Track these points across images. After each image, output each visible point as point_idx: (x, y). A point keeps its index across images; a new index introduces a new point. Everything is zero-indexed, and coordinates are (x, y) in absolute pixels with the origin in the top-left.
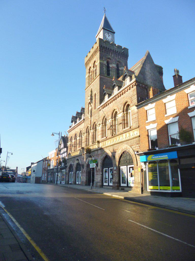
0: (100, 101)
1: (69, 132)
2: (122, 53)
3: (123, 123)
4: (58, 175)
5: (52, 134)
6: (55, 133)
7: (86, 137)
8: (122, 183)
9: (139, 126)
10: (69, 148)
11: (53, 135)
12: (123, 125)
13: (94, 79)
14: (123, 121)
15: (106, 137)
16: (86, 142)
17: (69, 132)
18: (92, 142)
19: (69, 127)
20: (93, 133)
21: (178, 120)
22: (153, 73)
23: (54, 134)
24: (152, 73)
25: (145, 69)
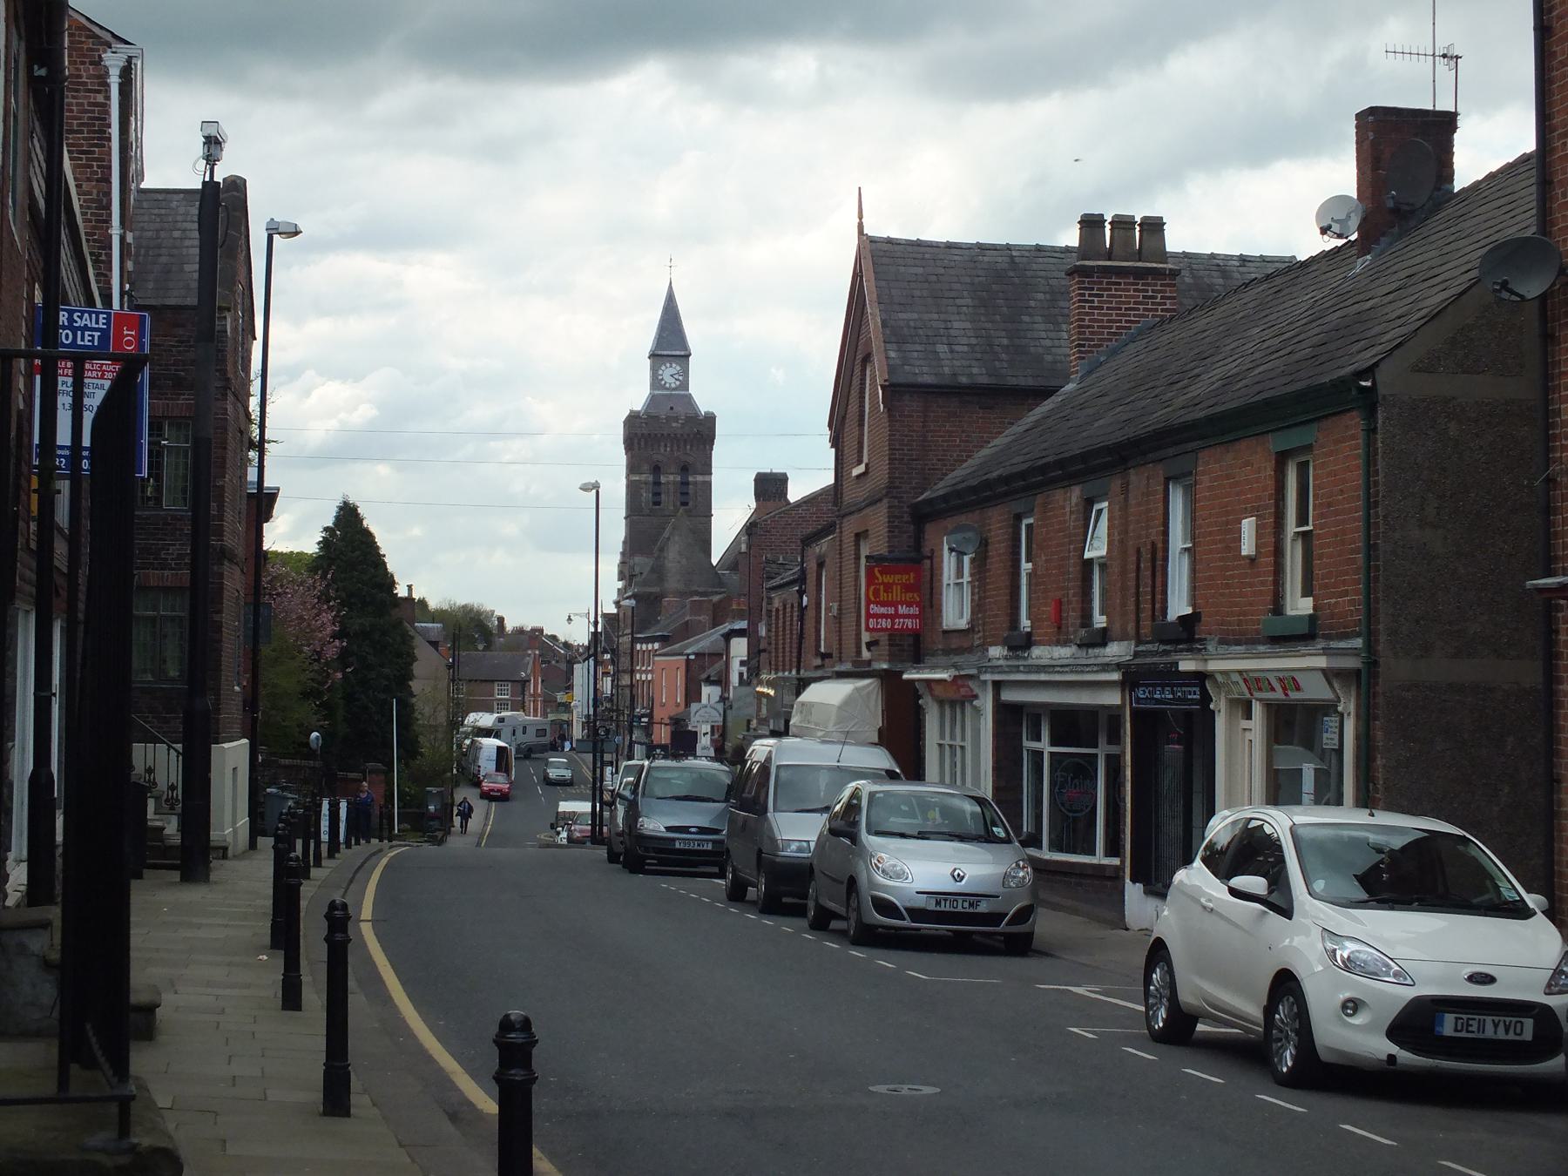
11: (569, 619)
25: (664, 558)
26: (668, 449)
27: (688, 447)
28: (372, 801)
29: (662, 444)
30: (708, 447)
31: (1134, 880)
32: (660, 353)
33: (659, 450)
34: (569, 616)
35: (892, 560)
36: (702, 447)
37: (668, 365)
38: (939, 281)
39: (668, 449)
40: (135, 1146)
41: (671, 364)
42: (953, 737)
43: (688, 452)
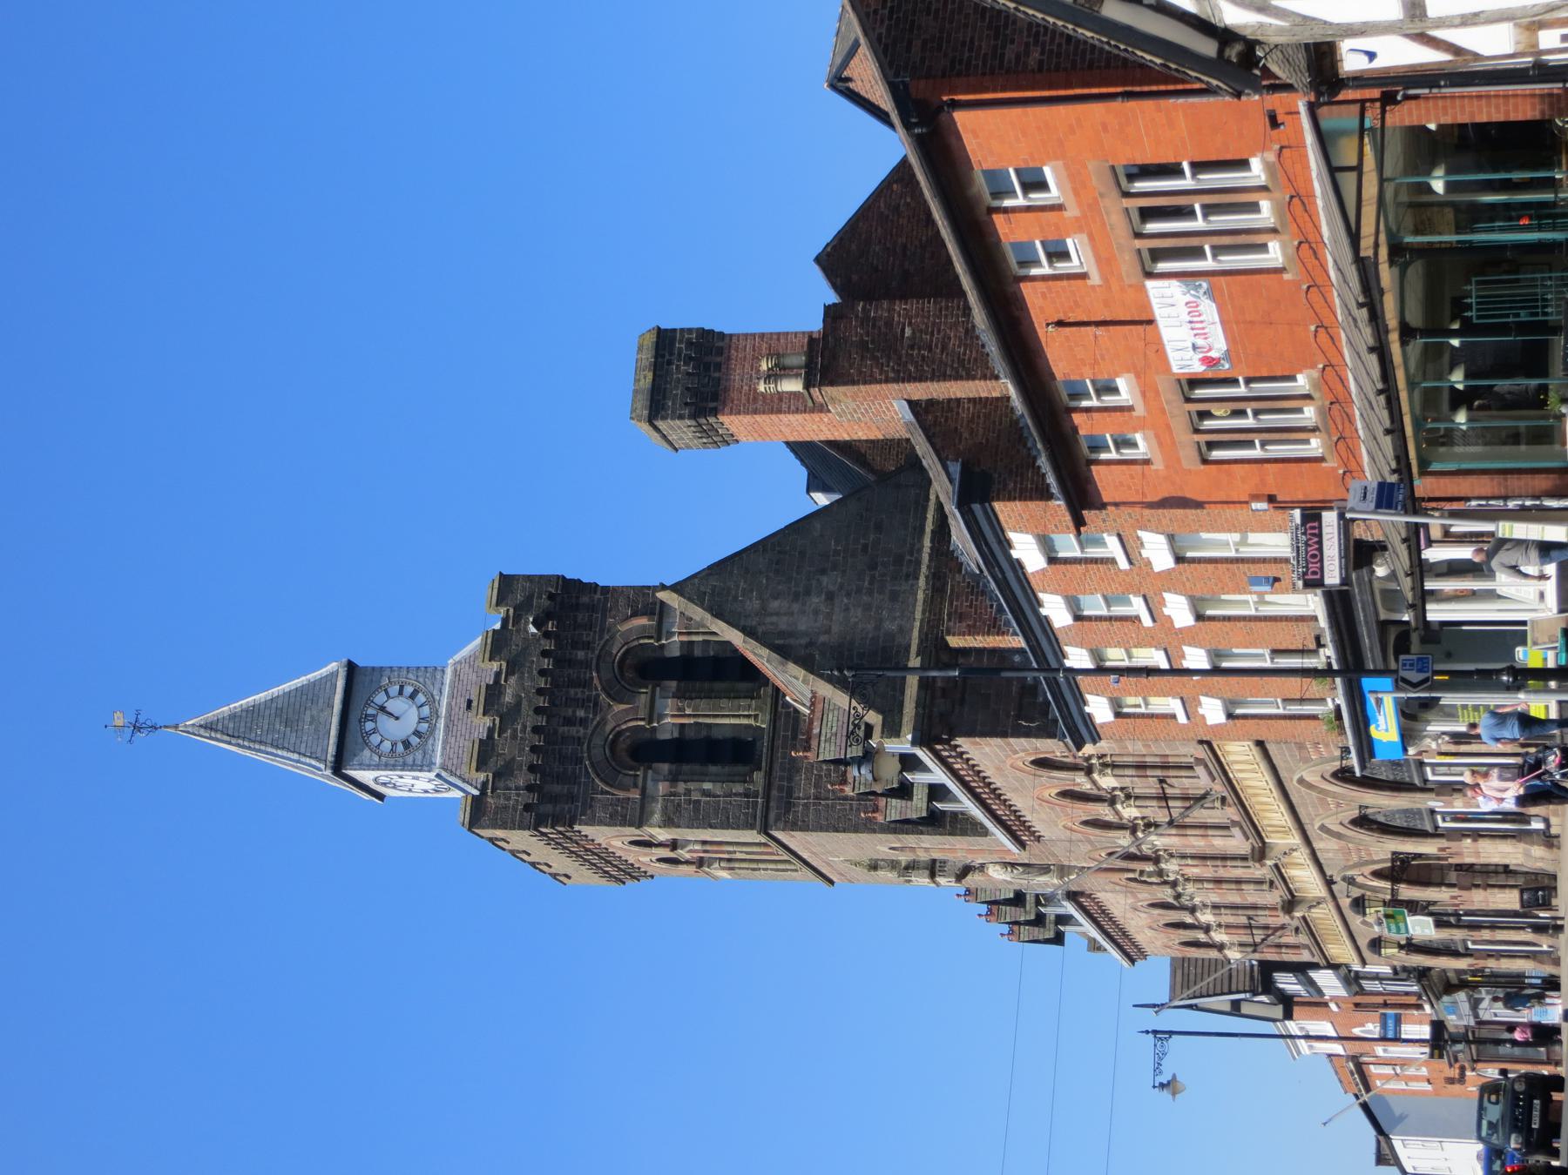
0: (964, 833)
1: (1132, 953)
2: (547, 635)
3: (1159, 773)
4: (1374, 662)
5: (1166, 1094)
6: (1157, 1069)
7: (1206, 885)
8: (1426, 343)
9: (1201, 742)
10: (1271, 955)
11: (1169, 1086)
12: (1172, 773)
13: (765, 845)
14: (1149, 772)
15: (1235, 823)
16: (1244, 887)
17: (1132, 953)
18: (1266, 887)
19: (1099, 955)
20: (1190, 862)
21: (1201, 647)
22: (823, 572)
23: (1164, 1079)
24: (825, 580)
25: (811, 644)
26: (581, 713)
27: (581, 654)
28: (1288, 1004)
29: (564, 729)
30: (585, 599)
31: (1383, 92)
32: (332, 750)
33: (579, 741)
34: (1162, 1086)
35: (1370, 582)
36: (582, 617)
37: (369, 726)
38: (270, 708)
39: (581, 713)
40: (804, 388)
41: (369, 734)
42: (1537, 307)
43: (593, 656)
